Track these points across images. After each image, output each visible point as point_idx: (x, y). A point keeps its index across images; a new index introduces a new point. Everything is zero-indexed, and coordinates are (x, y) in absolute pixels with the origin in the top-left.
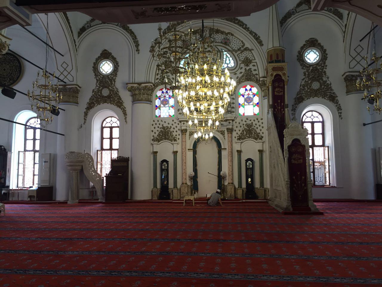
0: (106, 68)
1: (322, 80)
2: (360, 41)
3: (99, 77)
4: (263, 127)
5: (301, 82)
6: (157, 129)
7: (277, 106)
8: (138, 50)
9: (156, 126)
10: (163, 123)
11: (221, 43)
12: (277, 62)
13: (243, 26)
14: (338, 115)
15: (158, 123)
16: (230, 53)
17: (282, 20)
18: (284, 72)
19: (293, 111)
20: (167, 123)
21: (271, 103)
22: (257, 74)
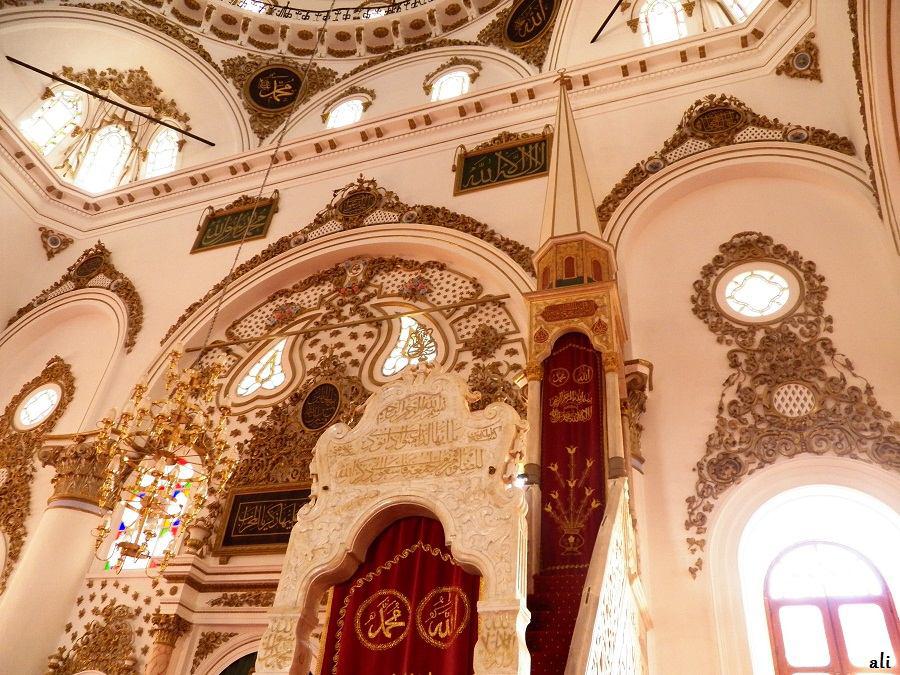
1: (820, 373)
5: (723, 395)
11: (400, 295)
18: (597, 320)
19: (694, 529)
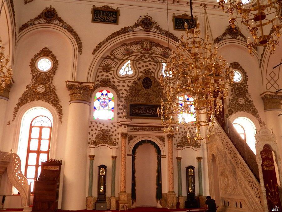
0: (44, 65)
2: (274, 68)
9: (94, 129)
11: (161, 55)
15: (96, 126)
20: (106, 125)
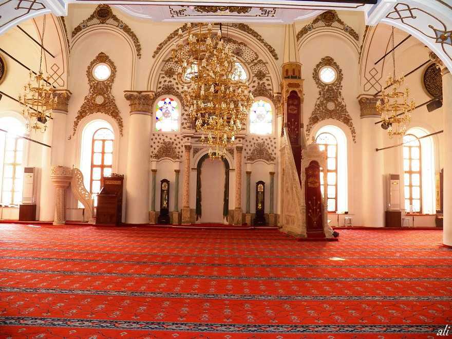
0: (102, 72)
1: (337, 100)
2: (375, 64)
3: (94, 82)
4: (275, 148)
6: (157, 144)
7: (290, 125)
8: (139, 55)
9: (156, 141)
10: (163, 138)
12: (293, 77)
13: (257, 37)
14: (352, 138)
15: (158, 138)
16: (242, 64)
17: (298, 34)
20: (169, 138)
21: (286, 121)
22: (270, 90)
